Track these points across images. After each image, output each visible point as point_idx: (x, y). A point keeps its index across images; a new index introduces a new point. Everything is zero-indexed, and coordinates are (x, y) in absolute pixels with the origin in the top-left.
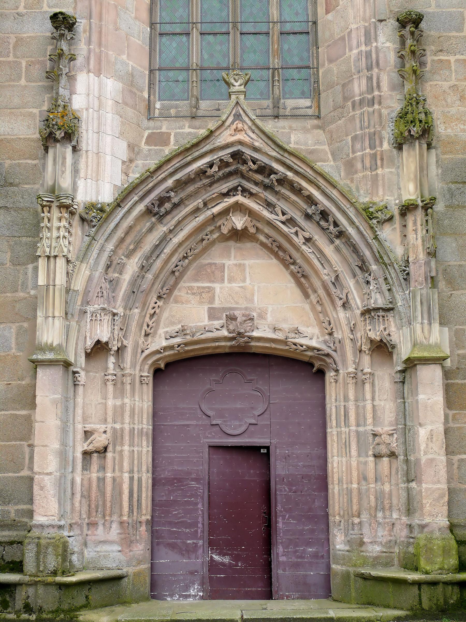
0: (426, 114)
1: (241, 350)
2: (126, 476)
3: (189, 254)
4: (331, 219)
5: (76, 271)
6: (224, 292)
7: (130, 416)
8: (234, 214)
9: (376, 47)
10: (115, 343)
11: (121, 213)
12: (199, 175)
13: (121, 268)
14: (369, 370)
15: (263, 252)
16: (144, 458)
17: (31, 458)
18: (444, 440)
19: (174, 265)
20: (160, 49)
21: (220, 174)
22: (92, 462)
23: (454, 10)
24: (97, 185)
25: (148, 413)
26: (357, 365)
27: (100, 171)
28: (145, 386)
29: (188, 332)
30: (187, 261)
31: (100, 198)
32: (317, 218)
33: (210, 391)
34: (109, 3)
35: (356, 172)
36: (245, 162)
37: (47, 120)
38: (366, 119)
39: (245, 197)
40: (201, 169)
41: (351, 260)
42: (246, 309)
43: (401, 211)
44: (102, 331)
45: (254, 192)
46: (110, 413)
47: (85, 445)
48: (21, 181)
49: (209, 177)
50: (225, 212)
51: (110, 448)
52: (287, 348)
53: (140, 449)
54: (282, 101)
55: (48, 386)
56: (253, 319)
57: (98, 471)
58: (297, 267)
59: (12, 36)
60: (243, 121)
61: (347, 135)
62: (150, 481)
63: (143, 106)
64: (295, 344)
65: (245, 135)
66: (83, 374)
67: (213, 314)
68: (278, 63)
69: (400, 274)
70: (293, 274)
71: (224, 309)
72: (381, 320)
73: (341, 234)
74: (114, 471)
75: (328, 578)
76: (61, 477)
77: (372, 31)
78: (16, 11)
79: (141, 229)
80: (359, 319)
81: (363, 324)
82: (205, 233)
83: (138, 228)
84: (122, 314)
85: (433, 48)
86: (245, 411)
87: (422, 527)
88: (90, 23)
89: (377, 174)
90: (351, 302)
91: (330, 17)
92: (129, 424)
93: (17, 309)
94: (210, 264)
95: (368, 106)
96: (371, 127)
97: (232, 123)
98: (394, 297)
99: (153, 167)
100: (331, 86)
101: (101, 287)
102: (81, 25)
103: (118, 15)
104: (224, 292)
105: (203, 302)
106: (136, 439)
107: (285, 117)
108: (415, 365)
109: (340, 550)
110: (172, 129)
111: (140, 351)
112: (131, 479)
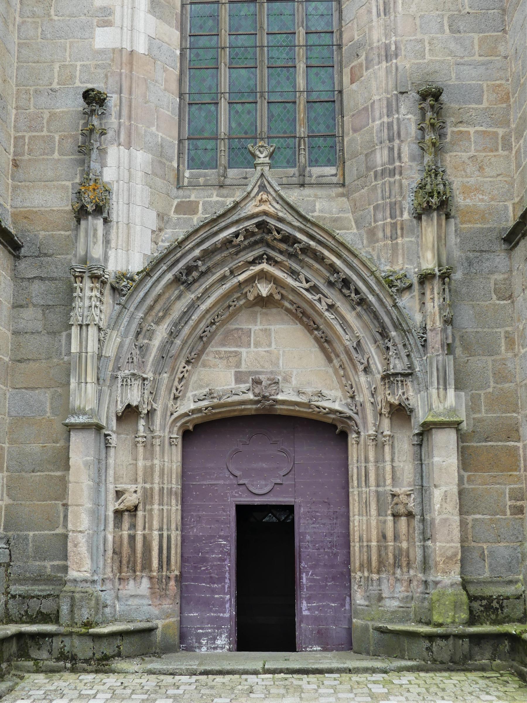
0: (445, 185)
1: (267, 413)
2: (156, 533)
3: (216, 320)
4: (352, 287)
5: (107, 338)
6: (251, 357)
7: (159, 476)
8: (260, 281)
9: (398, 119)
10: (145, 406)
11: (150, 282)
12: (225, 244)
13: (150, 335)
14: (389, 433)
15: (287, 318)
16: (173, 516)
17: (66, 517)
18: (458, 501)
19: (202, 330)
20: (189, 119)
21: (246, 243)
22: (123, 520)
23: (474, 82)
24: (128, 255)
25: (177, 473)
26: (378, 427)
27: (130, 242)
28: (174, 447)
29: (215, 395)
30: (214, 327)
31: (130, 268)
32: (340, 285)
33: (237, 452)
34: (138, 77)
35: (377, 241)
36: (270, 232)
37: (79, 193)
38: (387, 189)
39: (270, 265)
40: (227, 239)
41: (372, 326)
42: (271, 372)
43: (420, 279)
44: (132, 395)
45: (279, 260)
46: (140, 473)
47: (117, 504)
48: (55, 252)
49: (234, 246)
50: (251, 280)
51: (141, 507)
52: (310, 410)
53: (169, 508)
54: (308, 169)
55: (81, 451)
56: (278, 383)
57: (129, 529)
58: (320, 332)
59: (45, 111)
60: (268, 193)
61: (369, 205)
62: (179, 538)
63: (172, 177)
64: (318, 407)
65: (270, 206)
66: (114, 436)
67: (239, 378)
68: (304, 132)
69: (418, 341)
70: (316, 339)
71: (250, 373)
72: (400, 385)
73: (362, 302)
74: (144, 529)
75: (349, 630)
76: (93, 535)
77: (394, 103)
78: (50, 87)
79: (169, 298)
80: (379, 383)
81: (383, 388)
82: (232, 299)
83: (167, 295)
84: (152, 379)
85: (453, 119)
86: (262, 477)
87: (436, 583)
88: (121, 97)
89: (397, 243)
90: (373, 366)
91: (354, 86)
92: (159, 484)
93: (51, 376)
94: (237, 329)
95: (390, 177)
96: (392, 197)
97: (257, 194)
98: (412, 363)
99: (181, 237)
100: (355, 155)
101: (131, 353)
102: (113, 101)
103: (147, 88)
104: (251, 357)
105: (230, 366)
106: (165, 499)
107: (311, 185)
108: (431, 429)
109: (360, 605)
110: (200, 198)
111: (169, 414)
112: (161, 536)
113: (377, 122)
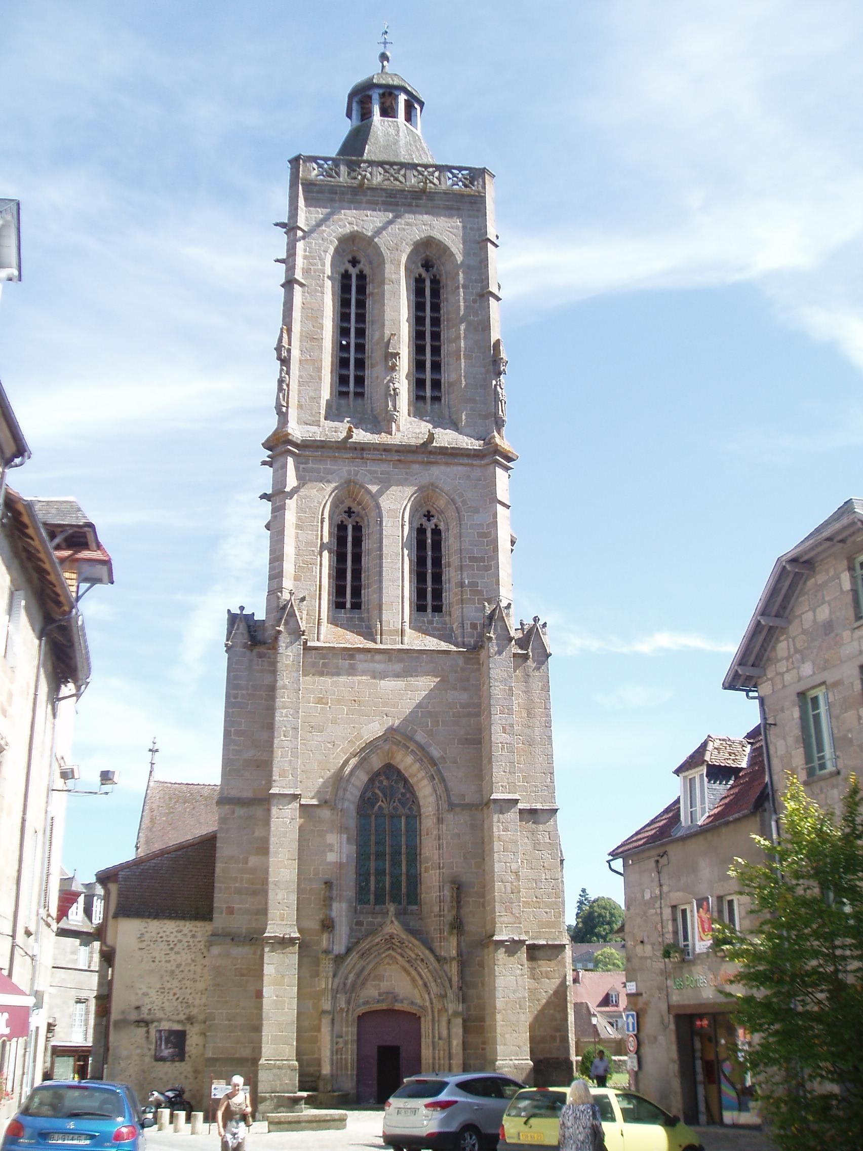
113: (435, 894)
